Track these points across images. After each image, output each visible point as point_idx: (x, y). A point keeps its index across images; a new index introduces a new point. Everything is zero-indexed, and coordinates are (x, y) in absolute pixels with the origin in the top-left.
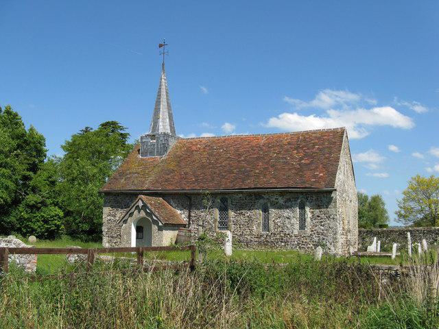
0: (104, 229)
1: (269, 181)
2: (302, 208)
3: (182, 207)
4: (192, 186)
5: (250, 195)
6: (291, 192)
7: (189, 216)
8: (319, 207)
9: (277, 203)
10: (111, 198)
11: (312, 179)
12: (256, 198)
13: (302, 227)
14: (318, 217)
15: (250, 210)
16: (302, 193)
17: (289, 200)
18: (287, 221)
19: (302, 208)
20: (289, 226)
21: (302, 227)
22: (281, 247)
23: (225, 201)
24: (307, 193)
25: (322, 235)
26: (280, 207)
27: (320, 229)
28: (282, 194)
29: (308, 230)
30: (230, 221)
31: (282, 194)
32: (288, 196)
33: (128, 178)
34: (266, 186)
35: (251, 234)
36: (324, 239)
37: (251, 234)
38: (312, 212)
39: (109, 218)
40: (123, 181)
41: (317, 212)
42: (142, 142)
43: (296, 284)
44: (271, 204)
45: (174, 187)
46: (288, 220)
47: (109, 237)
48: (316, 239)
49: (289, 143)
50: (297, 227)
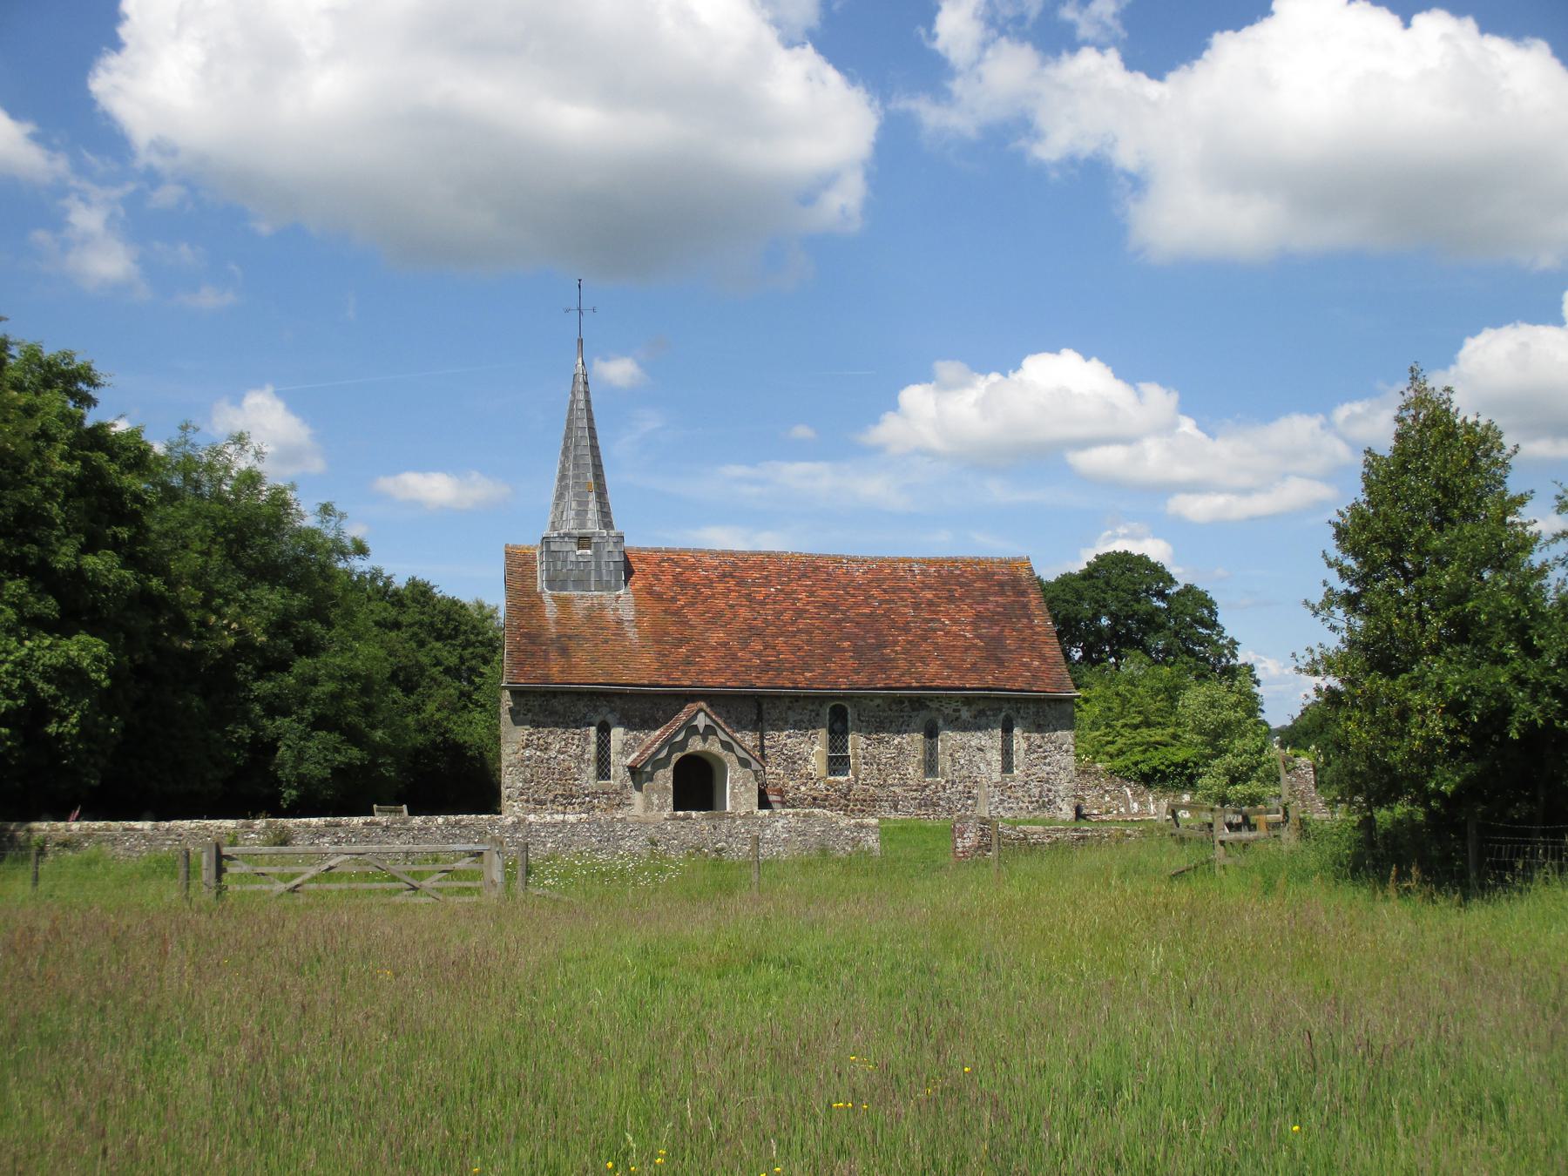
1: (933, 672)
2: (1007, 730)
4: (765, 678)
5: (900, 701)
6: (986, 698)
8: (1040, 728)
12: (920, 711)
13: (1007, 767)
15: (899, 732)
16: (1008, 699)
17: (982, 713)
18: (979, 755)
19: (1007, 730)
21: (1007, 767)
24: (1017, 700)
26: (965, 727)
27: (1042, 771)
28: (968, 701)
38: (1028, 739)
39: (527, 753)
48: (1036, 791)
50: (997, 766)
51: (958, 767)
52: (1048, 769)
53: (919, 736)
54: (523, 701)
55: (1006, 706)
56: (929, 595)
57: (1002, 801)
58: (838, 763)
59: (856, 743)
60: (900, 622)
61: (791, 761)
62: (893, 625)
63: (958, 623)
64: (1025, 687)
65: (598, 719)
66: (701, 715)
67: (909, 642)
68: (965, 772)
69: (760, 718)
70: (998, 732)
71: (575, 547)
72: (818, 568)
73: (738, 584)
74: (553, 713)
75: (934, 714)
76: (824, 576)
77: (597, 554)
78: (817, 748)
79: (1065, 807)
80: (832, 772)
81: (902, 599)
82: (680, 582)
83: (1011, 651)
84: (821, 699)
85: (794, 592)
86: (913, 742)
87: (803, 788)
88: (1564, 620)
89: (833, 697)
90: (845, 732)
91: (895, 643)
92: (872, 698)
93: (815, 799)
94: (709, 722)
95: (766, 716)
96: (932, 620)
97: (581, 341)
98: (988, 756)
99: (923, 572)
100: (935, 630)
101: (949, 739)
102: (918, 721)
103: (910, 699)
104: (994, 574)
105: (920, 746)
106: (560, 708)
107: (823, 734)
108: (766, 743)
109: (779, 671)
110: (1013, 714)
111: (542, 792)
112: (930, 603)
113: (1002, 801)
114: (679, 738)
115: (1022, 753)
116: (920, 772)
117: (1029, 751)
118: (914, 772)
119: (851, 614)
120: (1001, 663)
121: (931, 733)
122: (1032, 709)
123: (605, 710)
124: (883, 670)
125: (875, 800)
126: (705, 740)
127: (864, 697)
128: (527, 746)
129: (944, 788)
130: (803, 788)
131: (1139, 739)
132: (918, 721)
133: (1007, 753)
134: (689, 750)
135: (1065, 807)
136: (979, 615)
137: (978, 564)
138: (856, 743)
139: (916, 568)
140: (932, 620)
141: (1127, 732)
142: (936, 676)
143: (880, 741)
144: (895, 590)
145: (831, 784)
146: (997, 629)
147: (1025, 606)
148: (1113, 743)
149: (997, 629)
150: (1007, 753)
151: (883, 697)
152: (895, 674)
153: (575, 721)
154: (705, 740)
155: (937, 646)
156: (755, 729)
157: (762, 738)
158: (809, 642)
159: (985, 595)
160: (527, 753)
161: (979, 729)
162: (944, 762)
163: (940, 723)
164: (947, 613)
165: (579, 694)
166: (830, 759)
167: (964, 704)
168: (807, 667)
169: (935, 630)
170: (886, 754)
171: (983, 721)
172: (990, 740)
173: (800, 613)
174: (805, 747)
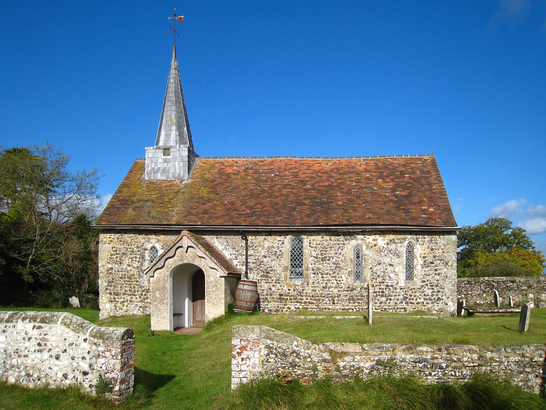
0: (102, 283)
4: (249, 220)
9: (375, 245)
14: (432, 263)
18: (390, 269)
20: (392, 275)
21: (410, 276)
22: (381, 303)
29: (418, 282)
30: (307, 269)
33: (136, 207)
35: (338, 286)
36: (439, 292)
37: (338, 286)
39: (110, 266)
40: (130, 211)
43: (293, 401)
44: (367, 246)
45: (221, 221)
47: (110, 294)
48: (429, 292)
49: (366, 171)
50: (402, 277)
72: (303, 164)
101: (311, 244)
112: (368, 179)
135: (450, 303)
142: (360, 218)
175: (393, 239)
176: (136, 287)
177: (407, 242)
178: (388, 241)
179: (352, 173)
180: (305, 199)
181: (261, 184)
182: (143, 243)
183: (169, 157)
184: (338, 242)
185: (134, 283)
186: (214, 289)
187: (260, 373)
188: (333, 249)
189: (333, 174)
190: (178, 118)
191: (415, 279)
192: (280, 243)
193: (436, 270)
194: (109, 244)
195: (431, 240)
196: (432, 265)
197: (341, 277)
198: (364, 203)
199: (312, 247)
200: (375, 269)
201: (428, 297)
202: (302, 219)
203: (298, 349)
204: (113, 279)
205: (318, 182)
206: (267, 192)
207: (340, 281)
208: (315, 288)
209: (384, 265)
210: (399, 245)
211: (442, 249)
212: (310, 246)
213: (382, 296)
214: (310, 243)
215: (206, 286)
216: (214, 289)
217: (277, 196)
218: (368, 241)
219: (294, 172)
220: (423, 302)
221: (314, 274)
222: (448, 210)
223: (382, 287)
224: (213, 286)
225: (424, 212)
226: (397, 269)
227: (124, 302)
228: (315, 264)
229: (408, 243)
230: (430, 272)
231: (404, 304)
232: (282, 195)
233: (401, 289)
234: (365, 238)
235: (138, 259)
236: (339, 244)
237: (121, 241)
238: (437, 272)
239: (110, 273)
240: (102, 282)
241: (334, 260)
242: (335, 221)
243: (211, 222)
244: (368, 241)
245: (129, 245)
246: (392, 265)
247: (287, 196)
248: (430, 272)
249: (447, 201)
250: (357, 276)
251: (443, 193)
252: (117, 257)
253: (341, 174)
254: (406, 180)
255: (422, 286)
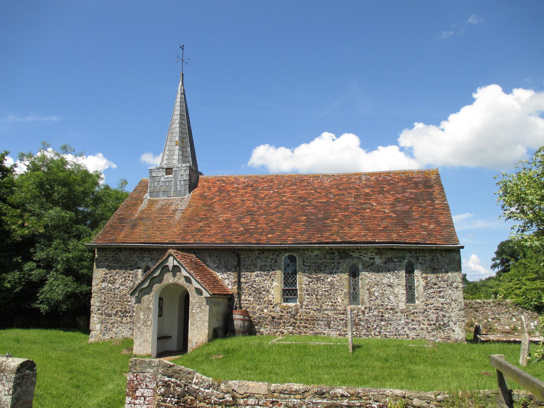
0: (95, 302)
1: (356, 233)
2: (410, 271)
3: (226, 269)
4: (242, 238)
5: (331, 251)
6: (392, 249)
7: (239, 283)
8: (434, 271)
9: (372, 264)
10: (110, 255)
11: (418, 234)
12: (345, 258)
13: (411, 298)
15: (331, 273)
16: (410, 250)
17: (390, 260)
18: (388, 290)
19: (410, 271)
21: (411, 298)
23: (291, 260)
24: (416, 250)
25: (442, 310)
26: (378, 270)
27: (438, 302)
28: (380, 251)
31: (380, 251)
32: (390, 255)
34: (355, 239)
38: (426, 278)
39: (104, 285)
41: (432, 277)
42: (152, 177)
44: (363, 265)
46: (386, 287)
48: (434, 317)
50: (403, 298)
51: (373, 298)
52: (442, 300)
53: (345, 276)
54: (103, 254)
55: (408, 255)
56: (367, 191)
57: (407, 323)
58: (289, 293)
59: (302, 280)
60: (343, 205)
61: (258, 292)
62: (339, 207)
63: (384, 205)
64: (420, 240)
65: (143, 265)
66: (171, 258)
67: (344, 216)
68: (378, 302)
69: (239, 265)
70: (403, 273)
71: (164, 174)
72: (303, 180)
73: (253, 190)
74: (119, 261)
75: (356, 261)
76: (305, 184)
77: (175, 177)
78: (275, 284)
79: (457, 329)
80: (286, 300)
81: (349, 193)
82: (221, 190)
83: (414, 219)
84: (277, 251)
85: (284, 192)
86: (341, 279)
87: (265, 311)
88: (286, 405)
89: (286, 250)
90: (295, 273)
91: (335, 217)
92: (313, 250)
93: (273, 318)
94: (176, 263)
95: (243, 263)
96: (365, 204)
97: (183, 74)
98: (396, 290)
99: (367, 180)
100: (365, 209)
101: (366, 278)
102: (345, 266)
103: (339, 250)
104: (413, 178)
105: (346, 283)
106: (123, 258)
107: (279, 274)
108: (243, 280)
109: (252, 234)
110: (413, 261)
111: (109, 309)
112: (367, 194)
113: (407, 323)
114: (157, 274)
115: (421, 289)
116: (346, 301)
117: (427, 287)
118: (341, 299)
119: (314, 202)
120: (406, 227)
121: (354, 274)
122: (428, 257)
123: (147, 259)
124: (320, 231)
125: (314, 320)
126: (174, 276)
127: (307, 249)
128: (104, 281)
129: (363, 312)
130: (265, 311)
131: (534, 286)
132: (345, 266)
133: (410, 288)
134: (165, 282)
135: (457, 329)
136: (397, 200)
137: (404, 173)
138: (302, 280)
139: (363, 178)
140: (365, 204)
141: (528, 283)
142: (356, 235)
143: (318, 279)
144: (346, 189)
145: (284, 308)
146: (407, 207)
147: (431, 194)
148: (520, 288)
149: (407, 207)
150: (410, 288)
151: (319, 249)
152: (327, 234)
153: (131, 266)
154: (174, 276)
155: (363, 218)
156: (236, 271)
157: (239, 277)
158: (280, 218)
159: (404, 189)
160: (104, 285)
161: (389, 271)
162: (363, 294)
163: (360, 267)
164: (376, 199)
165: (133, 250)
166: (284, 291)
167: (377, 254)
168: (272, 231)
169: (365, 209)
170: (322, 288)
171: (391, 265)
172: (397, 279)
173: (282, 203)
174: (267, 284)
175: (391, 258)
176: (127, 307)
177: (406, 261)
178: (386, 260)
179: (351, 188)
180: (301, 216)
181: (258, 201)
182: (137, 262)
183: (171, 176)
184: (333, 261)
185: (126, 303)
186: (198, 310)
187: (386, 381)
188: (327, 268)
189: (333, 191)
190: (182, 139)
191: (417, 302)
192: (273, 261)
193: (440, 292)
194: (104, 262)
195: (433, 259)
196: (436, 286)
197: (337, 299)
198: (361, 219)
199: (306, 266)
200: (372, 290)
201: (432, 322)
202: (294, 237)
203: (197, 387)
204: (105, 299)
205: (316, 199)
206: (263, 209)
207: (335, 303)
208: (309, 310)
209: (383, 286)
210: (398, 263)
211: (445, 269)
212: (304, 265)
213: (382, 320)
214: (303, 262)
215: (190, 307)
216: (198, 310)
217: (273, 214)
218: (364, 259)
219: (293, 189)
220: (427, 328)
221: (308, 294)
222: (450, 225)
223: (381, 310)
224: (198, 307)
225: (425, 229)
226: (396, 290)
227: (114, 323)
228: (309, 284)
229: (408, 262)
230: (434, 295)
231: (405, 329)
232: (277, 212)
233: (402, 312)
234: (361, 257)
235: (131, 279)
236: (333, 263)
237: (116, 260)
238: (441, 294)
239: (103, 293)
240: (94, 303)
241: (329, 280)
242: (327, 239)
243: (205, 240)
244: (364, 259)
245: (123, 264)
246: (391, 286)
247: (282, 213)
248: (434, 295)
249: (449, 216)
250: (353, 297)
251: (446, 208)
252: (110, 277)
253: (340, 190)
254: (406, 195)
255: (425, 310)
